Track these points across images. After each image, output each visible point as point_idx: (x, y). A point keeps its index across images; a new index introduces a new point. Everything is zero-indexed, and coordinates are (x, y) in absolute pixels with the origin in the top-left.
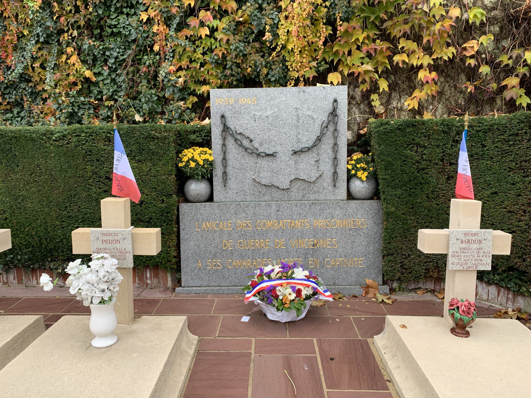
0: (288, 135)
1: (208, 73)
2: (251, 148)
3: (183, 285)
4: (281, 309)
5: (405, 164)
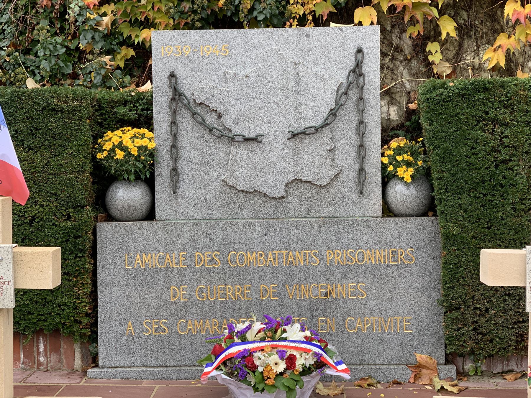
1: (153, 7)
2: (220, 128)
3: (100, 364)
4: (260, 389)
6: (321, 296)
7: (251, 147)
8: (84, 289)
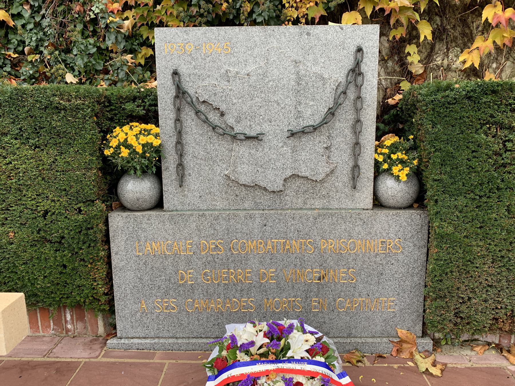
0: (282, 106)
1: (166, 12)
2: (223, 126)
3: (119, 335)
5: (475, 157)
6: (315, 280)
7: (252, 145)
8: (100, 273)
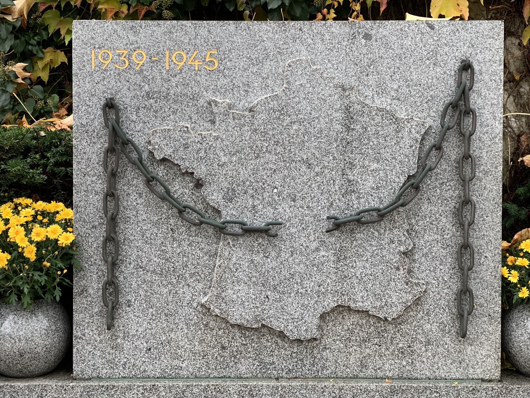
0: (317, 169)
2: (199, 207)
